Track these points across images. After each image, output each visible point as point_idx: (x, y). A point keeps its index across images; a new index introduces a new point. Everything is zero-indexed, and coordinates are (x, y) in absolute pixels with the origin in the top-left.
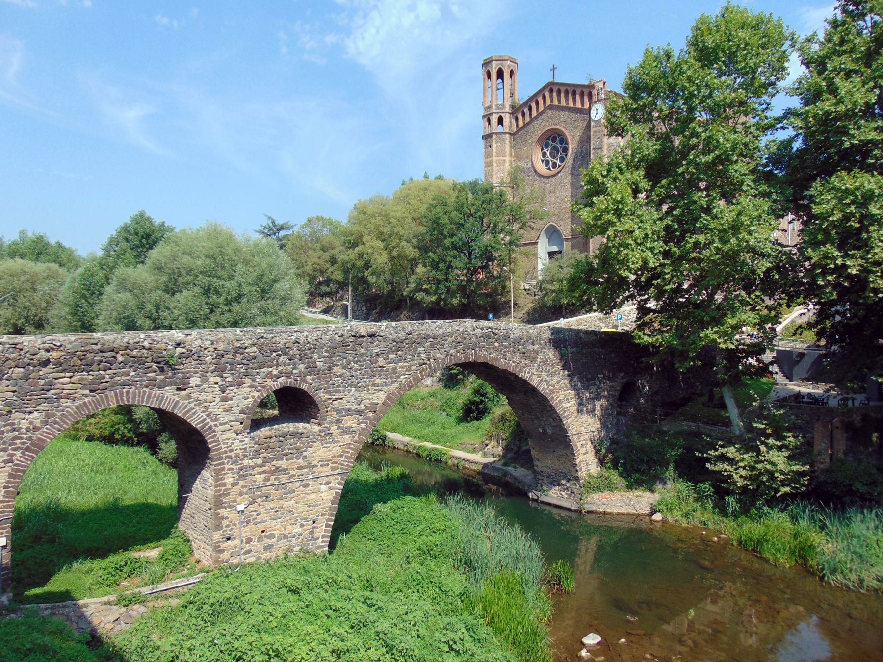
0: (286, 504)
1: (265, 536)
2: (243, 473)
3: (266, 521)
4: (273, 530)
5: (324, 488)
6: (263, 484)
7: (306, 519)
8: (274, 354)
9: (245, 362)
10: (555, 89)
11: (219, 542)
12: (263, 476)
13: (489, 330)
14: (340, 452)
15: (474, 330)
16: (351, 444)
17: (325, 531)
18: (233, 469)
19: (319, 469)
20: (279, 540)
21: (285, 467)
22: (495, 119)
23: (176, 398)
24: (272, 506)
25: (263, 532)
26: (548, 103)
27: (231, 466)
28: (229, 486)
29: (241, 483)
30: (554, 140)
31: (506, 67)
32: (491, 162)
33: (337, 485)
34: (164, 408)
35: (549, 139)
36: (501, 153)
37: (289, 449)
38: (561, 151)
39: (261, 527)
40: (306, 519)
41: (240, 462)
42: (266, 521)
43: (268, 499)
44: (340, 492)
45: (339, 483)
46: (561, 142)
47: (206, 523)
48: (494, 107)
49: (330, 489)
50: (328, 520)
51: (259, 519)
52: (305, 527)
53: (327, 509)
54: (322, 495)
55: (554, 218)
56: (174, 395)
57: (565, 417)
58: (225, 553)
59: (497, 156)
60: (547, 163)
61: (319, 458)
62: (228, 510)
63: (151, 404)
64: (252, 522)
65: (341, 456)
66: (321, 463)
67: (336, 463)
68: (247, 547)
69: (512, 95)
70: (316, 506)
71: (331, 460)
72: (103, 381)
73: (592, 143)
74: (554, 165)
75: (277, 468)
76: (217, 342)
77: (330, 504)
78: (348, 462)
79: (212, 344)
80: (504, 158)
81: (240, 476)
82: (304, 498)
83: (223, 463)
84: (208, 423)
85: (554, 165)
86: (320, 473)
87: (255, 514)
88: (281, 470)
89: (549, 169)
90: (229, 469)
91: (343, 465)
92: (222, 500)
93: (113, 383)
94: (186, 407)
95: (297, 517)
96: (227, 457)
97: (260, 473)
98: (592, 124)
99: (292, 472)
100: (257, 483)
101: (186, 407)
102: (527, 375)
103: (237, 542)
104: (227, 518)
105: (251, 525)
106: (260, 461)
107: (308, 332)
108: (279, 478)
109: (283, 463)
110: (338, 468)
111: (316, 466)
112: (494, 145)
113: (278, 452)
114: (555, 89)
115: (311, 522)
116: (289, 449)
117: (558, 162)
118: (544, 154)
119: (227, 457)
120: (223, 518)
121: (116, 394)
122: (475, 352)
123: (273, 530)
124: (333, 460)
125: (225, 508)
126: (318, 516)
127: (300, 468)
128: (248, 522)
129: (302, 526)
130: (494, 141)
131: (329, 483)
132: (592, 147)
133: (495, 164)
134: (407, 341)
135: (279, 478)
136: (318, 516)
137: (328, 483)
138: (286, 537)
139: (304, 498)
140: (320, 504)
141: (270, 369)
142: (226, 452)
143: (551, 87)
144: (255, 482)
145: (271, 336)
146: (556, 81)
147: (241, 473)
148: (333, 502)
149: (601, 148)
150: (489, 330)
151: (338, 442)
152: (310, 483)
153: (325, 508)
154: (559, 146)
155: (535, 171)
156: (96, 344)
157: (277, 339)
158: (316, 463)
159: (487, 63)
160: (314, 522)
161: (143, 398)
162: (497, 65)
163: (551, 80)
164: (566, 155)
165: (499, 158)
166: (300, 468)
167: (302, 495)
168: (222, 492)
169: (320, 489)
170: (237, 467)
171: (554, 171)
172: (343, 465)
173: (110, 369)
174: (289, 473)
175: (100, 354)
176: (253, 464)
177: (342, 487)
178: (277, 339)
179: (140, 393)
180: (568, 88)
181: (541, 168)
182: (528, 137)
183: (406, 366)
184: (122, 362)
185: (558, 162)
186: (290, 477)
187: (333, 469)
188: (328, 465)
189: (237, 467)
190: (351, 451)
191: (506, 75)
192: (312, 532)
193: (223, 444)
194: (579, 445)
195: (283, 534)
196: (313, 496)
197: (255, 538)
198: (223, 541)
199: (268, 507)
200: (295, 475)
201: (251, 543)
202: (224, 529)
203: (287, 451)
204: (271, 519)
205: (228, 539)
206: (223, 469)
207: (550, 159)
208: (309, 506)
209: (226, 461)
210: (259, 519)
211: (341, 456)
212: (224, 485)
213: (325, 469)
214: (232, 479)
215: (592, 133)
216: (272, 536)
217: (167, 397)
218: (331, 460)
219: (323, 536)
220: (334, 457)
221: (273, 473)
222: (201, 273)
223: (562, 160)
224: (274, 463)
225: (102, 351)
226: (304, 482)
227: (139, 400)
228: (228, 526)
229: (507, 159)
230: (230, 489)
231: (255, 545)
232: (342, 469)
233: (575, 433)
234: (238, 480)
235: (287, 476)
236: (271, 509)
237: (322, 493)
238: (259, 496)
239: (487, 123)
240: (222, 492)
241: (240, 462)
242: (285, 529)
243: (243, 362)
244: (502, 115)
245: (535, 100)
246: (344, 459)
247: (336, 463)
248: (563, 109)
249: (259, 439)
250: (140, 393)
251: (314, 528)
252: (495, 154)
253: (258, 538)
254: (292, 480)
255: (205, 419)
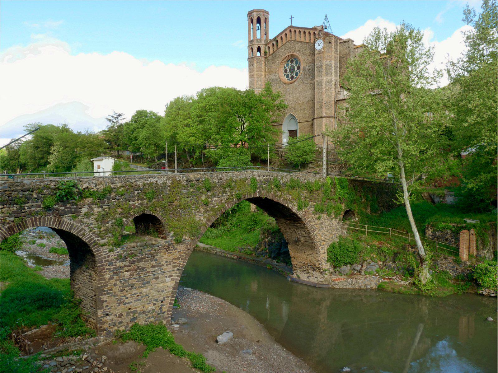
0: (144, 290)
1: (131, 312)
2: (116, 272)
3: (131, 302)
4: (136, 308)
5: (168, 279)
6: (129, 278)
7: (156, 300)
8: (136, 192)
9: (117, 197)
10: (293, 30)
11: (101, 317)
12: (129, 273)
13: (268, 177)
14: (178, 256)
15: (259, 177)
16: (185, 250)
17: (169, 307)
18: (110, 269)
19: (165, 267)
20: (140, 314)
21: (143, 266)
22: (255, 49)
23: (72, 222)
24: (135, 292)
25: (129, 309)
26: (289, 38)
27: (108, 267)
28: (107, 280)
29: (115, 277)
30: (292, 62)
31: (263, 16)
32: (253, 75)
33: (176, 277)
34: (64, 229)
35: (288, 61)
36: (259, 70)
37: (146, 255)
38: (288, 70)
39: (128, 306)
40: (156, 300)
41: (114, 264)
42: (131, 302)
43: (133, 288)
44: (178, 281)
45: (178, 276)
46: (296, 63)
47: (91, 305)
48: (255, 41)
49: (172, 279)
50: (171, 300)
51: (127, 301)
52: (156, 305)
53: (170, 293)
54: (167, 284)
55: (293, 110)
56: (70, 220)
57: (312, 231)
58: (105, 324)
59: (257, 71)
60: (288, 76)
61: (165, 260)
62: (107, 296)
63: (53, 225)
64: (122, 303)
65: (179, 258)
66: (166, 263)
67: (176, 263)
68: (120, 320)
69: (266, 34)
70: (163, 291)
71: (172, 261)
72: (23, 211)
73: (316, 64)
74: (292, 78)
75: (138, 267)
76: (99, 185)
77: (172, 290)
78: (183, 262)
79: (96, 186)
80: (261, 73)
81: (114, 273)
82: (155, 286)
83: (103, 265)
84: (94, 238)
85: (292, 78)
86: (165, 269)
87: (124, 298)
88: (141, 269)
89: (289, 80)
90: (107, 269)
91: (180, 264)
92: (103, 289)
93: (30, 212)
94: (78, 229)
95: (151, 299)
96: (106, 261)
97: (127, 271)
98: (316, 52)
99: (148, 270)
100: (126, 278)
101: (78, 229)
102: (290, 205)
103: (111, 317)
104: (106, 301)
105: (122, 305)
106: (127, 263)
107: (158, 178)
108: (139, 274)
109: (142, 264)
110: (177, 266)
111: (164, 265)
112: (255, 65)
113: (139, 256)
114: (293, 30)
115: (160, 302)
116: (146, 255)
117: (294, 76)
118: (286, 71)
119: (106, 261)
120: (103, 301)
121: (32, 220)
122: (260, 190)
123: (136, 308)
124: (174, 261)
125: (105, 294)
126: (164, 298)
127: (153, 267)
128: (120, 303)
129: (154, 304)
130: (255, 62)
131: (171, 276)
132: (316, 67)
133: (255, 76)
134: (219, 184)
135: (139, 274)
136: (164, 298)
137: (171, 276)
138: (144, 312)
139: (155, 286)
140: (166, 290)
141: (134, 203)
142: (105, 258)
143: (291, 29)
144: (124, 276)
145: (134, 181)
146: (293, 25)
147: (115, 271)
148: (174, 288)
149: (321, 67)
150: (268, 177)
151: (176, 249)
152: (159, 276)
153: (169, 292)
154: (295, 65)
155: (280, 80)
156: (18, 186)
157: (138, 183)
158: (163, 263)
159: (250, 14)
160: (162, 302)
161: (50, 222)
162: (257, 15)
163: (290, 25)
164: (299, 71)
165: (258, 73)
166: (153, 267)
167: (154, 285)
168: (102, 284)
169: (165, 280)
170: (113, 267)
171: (291, 81)
172: (180, 264)
173: (28, 203)
174: (146, 270)
175: (21, 192)
176: (123, 265)
177: (179, 278)
178: (138, 183)
179: (48, 219)
180: (301, 30)
181: (284, 79)
182: (276, 60)
183: (218, 200)
184: (36, 198)
185: (294, 76)
186: (147, 272)
187: (174, 267)
188: (171, 264)
189: (113, 267)
190: (185, 255)
191: (262, 21)
192: (161, 308)
193: (104, 252)
194: (320, 248)
195: (142, 310)
196: (161, 285)
197: (124, 314)
198: (104, 317)
199: (133, 293)
200: (149, 272)
201: (122, 317)
202: (105, 308)
203: (145, 256)
204: (134, 301)
205: (107, 315)
206: (104, 269)
207: (289, 73)
208: (159, 292)
209: (105, 264)
210: (127, 301)
211: (179, 258)
212: (104, 279)
213: (169, 267)
214: (109, 275)
215: (316, 58)
216: (135, 312)
217: (66, 221)
218: (172, 261)
219: (168, 311)
220: (174, 259)
221: (136, 270)
222: (11, 160)
223: (297, 74)
224: (137, 264)
225: (22, 191)
226: (156, 276)
227: (47, 224)
228: (107, 306)
229: (263, 73)
230: (108, 282)
231: (125, 319)
232: (179, 266)
233: (318, 241)
234: (113, 276)
235: (144, 272)
236: (135, 294)
237: (167, 282)
238: (127, 286)
239: (251, 51)
240: (102, 284)
241: (114, 264)
242: (144, 307)
243: (116, 197)
244: (260, 46)
245: (280, 37)
246: (180, 260)
247: (176, 263)
248: (301, 42)
249: (127, 248)
250: (48, 219)
251: (162, 305)
252: (255, 70)
253: (127, 314)
254: (148, 275)
255: (91, 236)
